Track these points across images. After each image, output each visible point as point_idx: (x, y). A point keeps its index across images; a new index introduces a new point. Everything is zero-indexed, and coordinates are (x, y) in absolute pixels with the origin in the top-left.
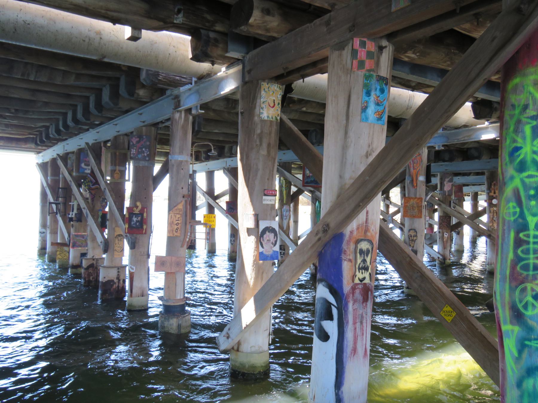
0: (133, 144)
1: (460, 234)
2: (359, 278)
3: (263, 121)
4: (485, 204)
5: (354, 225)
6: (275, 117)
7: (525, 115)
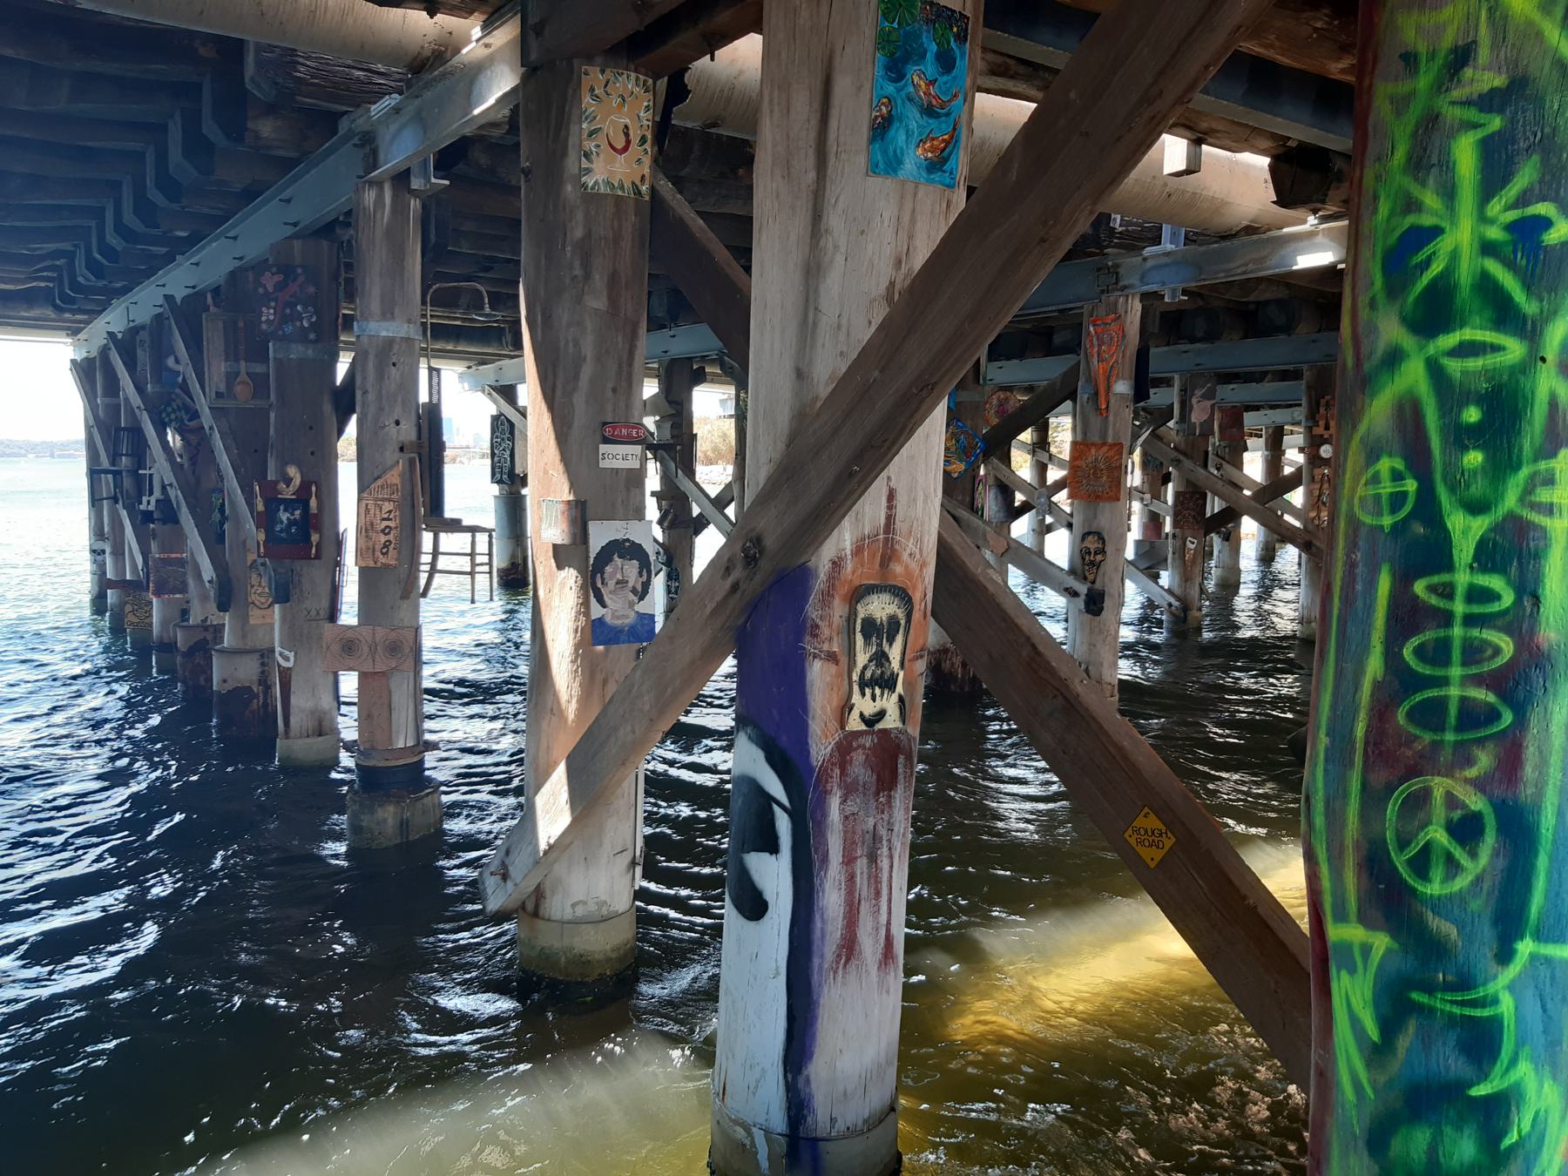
0: (267, 293)
1: (1232, 540)
2: (861, 714)
3: (592, 198)
4: (1300, 458)
5: (843, 538)
6: (633, 183)
7: (1456, 94)
